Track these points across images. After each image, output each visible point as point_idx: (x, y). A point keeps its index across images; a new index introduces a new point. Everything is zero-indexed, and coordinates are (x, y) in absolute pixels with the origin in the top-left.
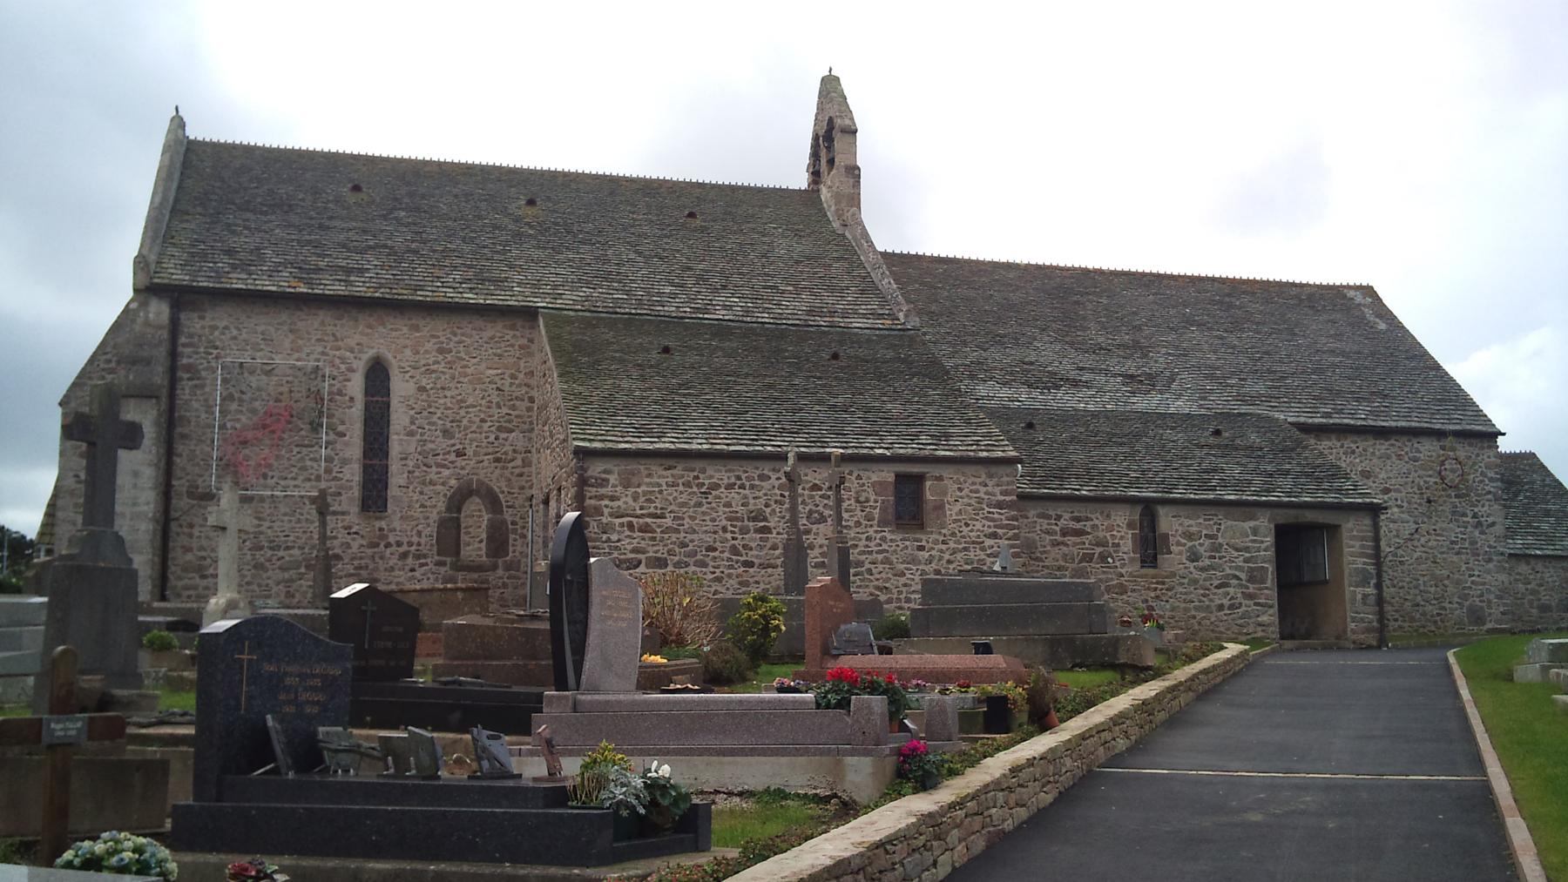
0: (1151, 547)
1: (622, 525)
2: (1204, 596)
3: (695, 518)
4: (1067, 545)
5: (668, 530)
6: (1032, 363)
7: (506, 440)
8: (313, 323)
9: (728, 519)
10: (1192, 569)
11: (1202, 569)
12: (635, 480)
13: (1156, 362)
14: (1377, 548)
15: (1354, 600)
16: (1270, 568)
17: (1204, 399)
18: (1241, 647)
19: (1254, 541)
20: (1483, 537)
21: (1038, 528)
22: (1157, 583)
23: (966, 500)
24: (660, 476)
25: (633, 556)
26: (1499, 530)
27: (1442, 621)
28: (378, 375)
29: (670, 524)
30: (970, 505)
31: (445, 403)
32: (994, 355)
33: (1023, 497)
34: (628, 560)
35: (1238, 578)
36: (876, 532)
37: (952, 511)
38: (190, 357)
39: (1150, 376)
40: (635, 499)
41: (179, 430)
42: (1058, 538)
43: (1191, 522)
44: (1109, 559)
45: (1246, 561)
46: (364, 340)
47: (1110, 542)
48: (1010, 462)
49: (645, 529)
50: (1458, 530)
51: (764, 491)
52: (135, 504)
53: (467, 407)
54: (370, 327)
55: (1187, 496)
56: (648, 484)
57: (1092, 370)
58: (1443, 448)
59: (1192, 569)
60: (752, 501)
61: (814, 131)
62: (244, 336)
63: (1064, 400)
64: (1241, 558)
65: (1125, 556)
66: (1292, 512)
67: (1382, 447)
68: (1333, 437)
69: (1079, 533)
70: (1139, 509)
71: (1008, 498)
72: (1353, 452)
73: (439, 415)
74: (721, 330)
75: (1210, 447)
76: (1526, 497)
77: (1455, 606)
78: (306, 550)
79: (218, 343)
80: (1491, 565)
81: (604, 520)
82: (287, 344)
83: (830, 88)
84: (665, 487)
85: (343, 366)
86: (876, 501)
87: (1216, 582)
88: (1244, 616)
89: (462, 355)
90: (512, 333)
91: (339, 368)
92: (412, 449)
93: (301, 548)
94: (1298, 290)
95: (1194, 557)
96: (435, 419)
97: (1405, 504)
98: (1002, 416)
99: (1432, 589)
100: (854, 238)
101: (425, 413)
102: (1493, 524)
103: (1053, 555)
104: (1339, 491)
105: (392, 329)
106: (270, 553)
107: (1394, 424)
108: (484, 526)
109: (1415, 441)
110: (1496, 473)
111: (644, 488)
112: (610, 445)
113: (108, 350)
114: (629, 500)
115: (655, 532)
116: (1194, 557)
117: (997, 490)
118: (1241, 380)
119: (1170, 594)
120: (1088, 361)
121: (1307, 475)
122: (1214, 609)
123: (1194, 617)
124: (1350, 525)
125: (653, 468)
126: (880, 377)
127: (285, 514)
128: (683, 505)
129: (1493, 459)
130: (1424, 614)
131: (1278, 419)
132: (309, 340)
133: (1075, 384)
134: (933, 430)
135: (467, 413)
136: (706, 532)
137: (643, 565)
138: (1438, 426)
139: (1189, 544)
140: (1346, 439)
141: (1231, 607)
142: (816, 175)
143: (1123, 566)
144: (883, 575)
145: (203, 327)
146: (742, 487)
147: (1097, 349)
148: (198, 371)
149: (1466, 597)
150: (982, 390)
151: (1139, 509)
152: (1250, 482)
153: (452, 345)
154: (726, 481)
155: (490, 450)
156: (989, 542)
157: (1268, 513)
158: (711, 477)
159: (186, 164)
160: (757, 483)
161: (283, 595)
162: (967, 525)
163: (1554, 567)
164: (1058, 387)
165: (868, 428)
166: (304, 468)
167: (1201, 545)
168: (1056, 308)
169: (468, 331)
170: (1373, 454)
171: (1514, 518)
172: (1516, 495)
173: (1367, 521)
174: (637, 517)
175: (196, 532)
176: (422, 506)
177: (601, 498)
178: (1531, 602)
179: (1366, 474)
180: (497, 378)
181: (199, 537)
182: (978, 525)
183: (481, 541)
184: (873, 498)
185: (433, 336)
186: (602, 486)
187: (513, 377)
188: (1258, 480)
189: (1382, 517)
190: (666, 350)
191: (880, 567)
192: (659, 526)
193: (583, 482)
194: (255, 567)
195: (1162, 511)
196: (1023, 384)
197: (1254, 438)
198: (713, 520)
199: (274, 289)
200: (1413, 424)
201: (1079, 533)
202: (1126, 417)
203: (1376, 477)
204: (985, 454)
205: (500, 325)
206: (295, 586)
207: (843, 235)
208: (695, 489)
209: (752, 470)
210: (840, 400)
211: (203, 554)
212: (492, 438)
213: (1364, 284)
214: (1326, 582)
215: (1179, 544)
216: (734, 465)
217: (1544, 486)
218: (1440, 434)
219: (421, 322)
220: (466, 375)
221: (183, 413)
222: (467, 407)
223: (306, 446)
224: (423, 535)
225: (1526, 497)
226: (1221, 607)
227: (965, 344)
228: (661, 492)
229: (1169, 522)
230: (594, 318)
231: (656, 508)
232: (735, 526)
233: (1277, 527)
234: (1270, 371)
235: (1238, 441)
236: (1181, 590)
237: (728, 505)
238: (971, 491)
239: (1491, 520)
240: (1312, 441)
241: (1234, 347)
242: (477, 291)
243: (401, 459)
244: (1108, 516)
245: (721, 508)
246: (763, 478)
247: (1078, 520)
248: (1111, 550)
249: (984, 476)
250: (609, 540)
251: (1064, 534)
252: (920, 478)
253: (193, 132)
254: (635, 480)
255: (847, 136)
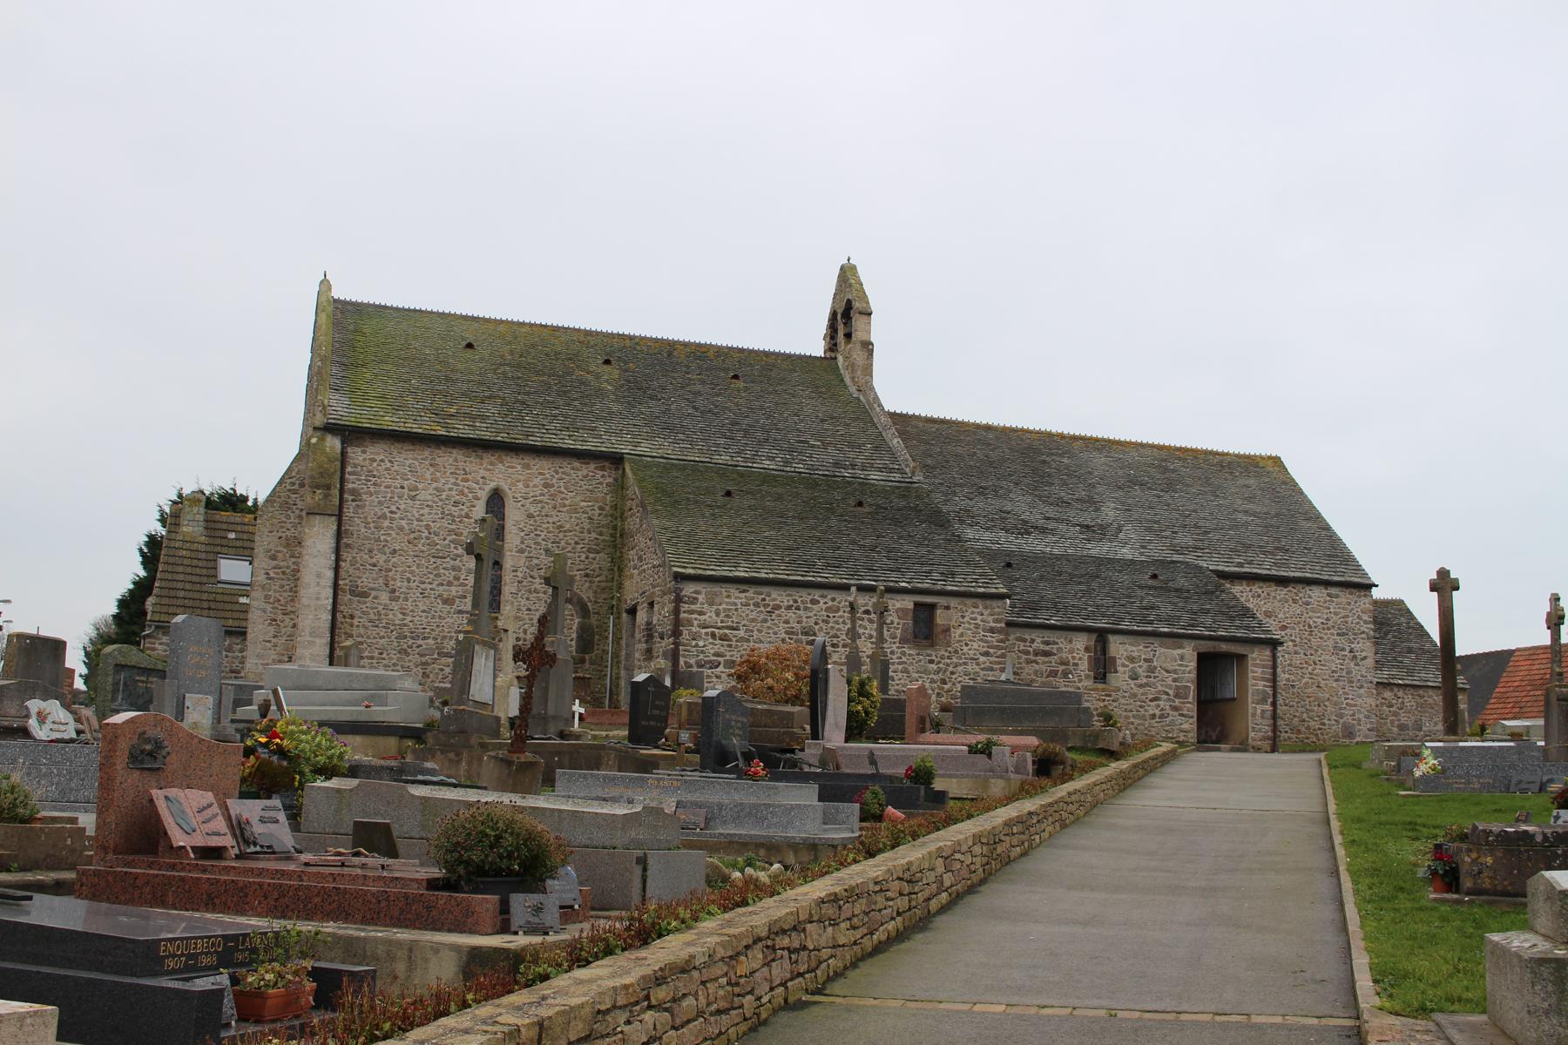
0: (1102, 667)
1: (707, 634)
2: (1141, 707)
3: (761, 631)
4: (1037, 663)
5: (741, 639)
6: (1009, 513)
7: (594, 559)
8: (449, 459)
9: (787, 633)
10: (1133, 686)
11: (1141, 686)
12: (717, 600)
13: (1107, 515)
14: (1274, 674)
15: (1254, 715)
16: (1193, 687)
17: (1143, 547)
18: (1173, 746)
19: (1181, 665)
20: (1357, 668)
21: (1016, 648)
22: (1107, 695)
23: (967, 625)
24: (736, 596)
25: (714, 658)
26: (1370, 662)
27: (1322, 734)
28: (496, 501)
29: (743, 635)
30: (970, 629)
31: (548, 528)
32: (979, 505)
33: (1009, 624)
34: (710, 662)
35: (1167, 694)
36: (898, 648)
37: (956, 633)
38: (353, 483)
39: (1102, 527)
40: (718, 614)
41: (345, 540)
42: (1032, 657)
43: (1134, 649)
44: (1070, 676)
45: (1175, 680)
46: (487, 474)
47: (1071, 661)
48: (1001, 597)
49: (724, 638)
50: (1338, 662)
51: (814, 612)
52: (318, 599)
53: (565, 532)
54: (492, 464)
55: (1131, 628)
56: (727, 603)
57: (1057, 520)
58: (1329, 595)
59: (1133, 686)
60: (805, 620)
61: (833, 307)
62: (396, 468)
63: (1035, 544)
64: (1170, 679)
65: (1082, 674)
66: (1202, 642)
67: (1282, 592)
68: (1244, 583)
69: (1047, 654)
70: (1094, 636)
71: (998, 625)
72: (1259, 596)
73: (543, 537)
74: (768, 478)
75: (1150, 588)
76: (1393, 637)
77: (1333, 722)
78: (439, 641)
79: (375, 473)
80: (1362, 691)
81: (694, 630)
82: (428, 476)
83: (847, 277)
84: (739, 606)
85: (470, 495)
86: (898, 624)
87: (1150, 697)
88: (1172, 723)
89: (562, 489)
90: (601, 473)
91: (467, 496)
92: (522, 563)
93: (435, 639)
94: (1221, 458)
95: (1134, 677)
96: (540, 540)
97: (1298, 640)
98: (989, 555)
99: (1316, 708)
100: (868, 400)
101: (532, 535)
102: (1365, 658)
103: (1027, 670)
104: (1247, 628)
105: (508, 467)
106: (412, 641)
107: (1292, 574)
108: (574, 628)
109: (1307, 588)
110: (1369, 617)
111: (724, 606)
112: (700, 572)
113: (293, 474)
114: (714, 616)
115: (731, 640)
116: (1134, 677)
117: (991, 618)
118: (1173, 532)
119: (1115, 704)
120: (1051, 512)
121: (1223, 613)
122: (1148, 717)
123: (1133, 724)
124: (1254, 655)
125: (732, 591)
126: (896, 522)
127: (424, 611)
128: (753, 620)
129: (1367, 605)
130: (1308, 728)
131: (1201, 567)
132: (445, 472)
133: (1043, 530)
134: (942, 569)
135: (565, 536)
136: (770, 642)
137: (721, 666)
138: (1326, 577)
139: (1131, 666)
140: (1254, 585)
141: (1162, 716)
142: (832, 346)
143: (1080, 681)
144: (902, 681)
145: (365, 459)
146: (798, 608)
147: (1061, 503)
148: (360, 495)
149: (1341, 716)
150: (970, 533)
151: (1094, 636)
152: (1179, 618)
153: (554, 481)
154: (786, 604)
155: (582, 567)
156: (982, 659)
157: (1193, 643)
158: (775, 600)
159: (337, 324)
160: (809, 605)
161: (421, 675)
162: (967, 645)
163: (1412, 694)
164: (1029, 533)
165: (891, 564)
166: (438, 575)
167: (1140, 667)
168: (1027, 466)
169: (568, 470)
170: (1275, 597)
171: (1383, 653)
172: (1386, 634)
173: (1268, 653)
174: (719, 628)
175: (355, 622)
176: (529, 610)
177: (692, 612)
178: (1392, 722)
179: (1268, 614)
180: (588, 509)
181: (358, 626)
182: (975, 645)
183: (572, 640)
184: (896, 621)
185: (540, 474)
186: (692, 603)
187: (601, 508)
188: (1186, 616)
189: (1279, 649)
190: (728, 494)
191: (900, 675)
192: (735, 636)
193: (678, 600)
194: (400, 653)
195: (1111, 638)
196: (1002, 529)
197: (1182, 582)
198: (775, 633)
199: (420, 431)
200: (1307, 575)
201: (1047, 654)
202: (1083, 560)
203: (1276, 617)
204: (982, 590)
205: (592, 466)
206: (430, 668)
207: (858, 399)
208: (762, 609)
209: (804, 596)
210: (867, 541)
211: (360, 639)
212: (583, 558)
213: (1274, 455)
214: (1234, 699)
215: (1124, 665)
216: (791, 591)
217: (1409, 628)
218: (1327, 584)
219: (532, 462)
220: (565, 506)
221: (347, 527)
222: (565, 532)
223: (441, 558)
224: (528, 632)
225: (1393, 637)
226: (1153, 716)
227: (955, 494)
228: (736, 610)
229: (1119, 648)
230: (667, 463)
231: (733, 622)
232: (791, 639)
233: (1199, 654)
234: (1196, 526)
235: (1170, 584)
236: (1123, 701)
237: (787, 622)
238: (971, 619)
239: (1364, 654)
240: (1228, 586)
241: (1168, 505)
242: (574, 438)
243: (514, 571)
244: (1071, 641)
245: (781, 624)
246: (814, 602)
247: (1047, 643)
248: (1072, 668)
249: (981, 607)
250: (697, 645)
251: (1036, 655)
252: (933, 607)
253: (339, 293)
254: (717, 600)
255: (863, 316)
